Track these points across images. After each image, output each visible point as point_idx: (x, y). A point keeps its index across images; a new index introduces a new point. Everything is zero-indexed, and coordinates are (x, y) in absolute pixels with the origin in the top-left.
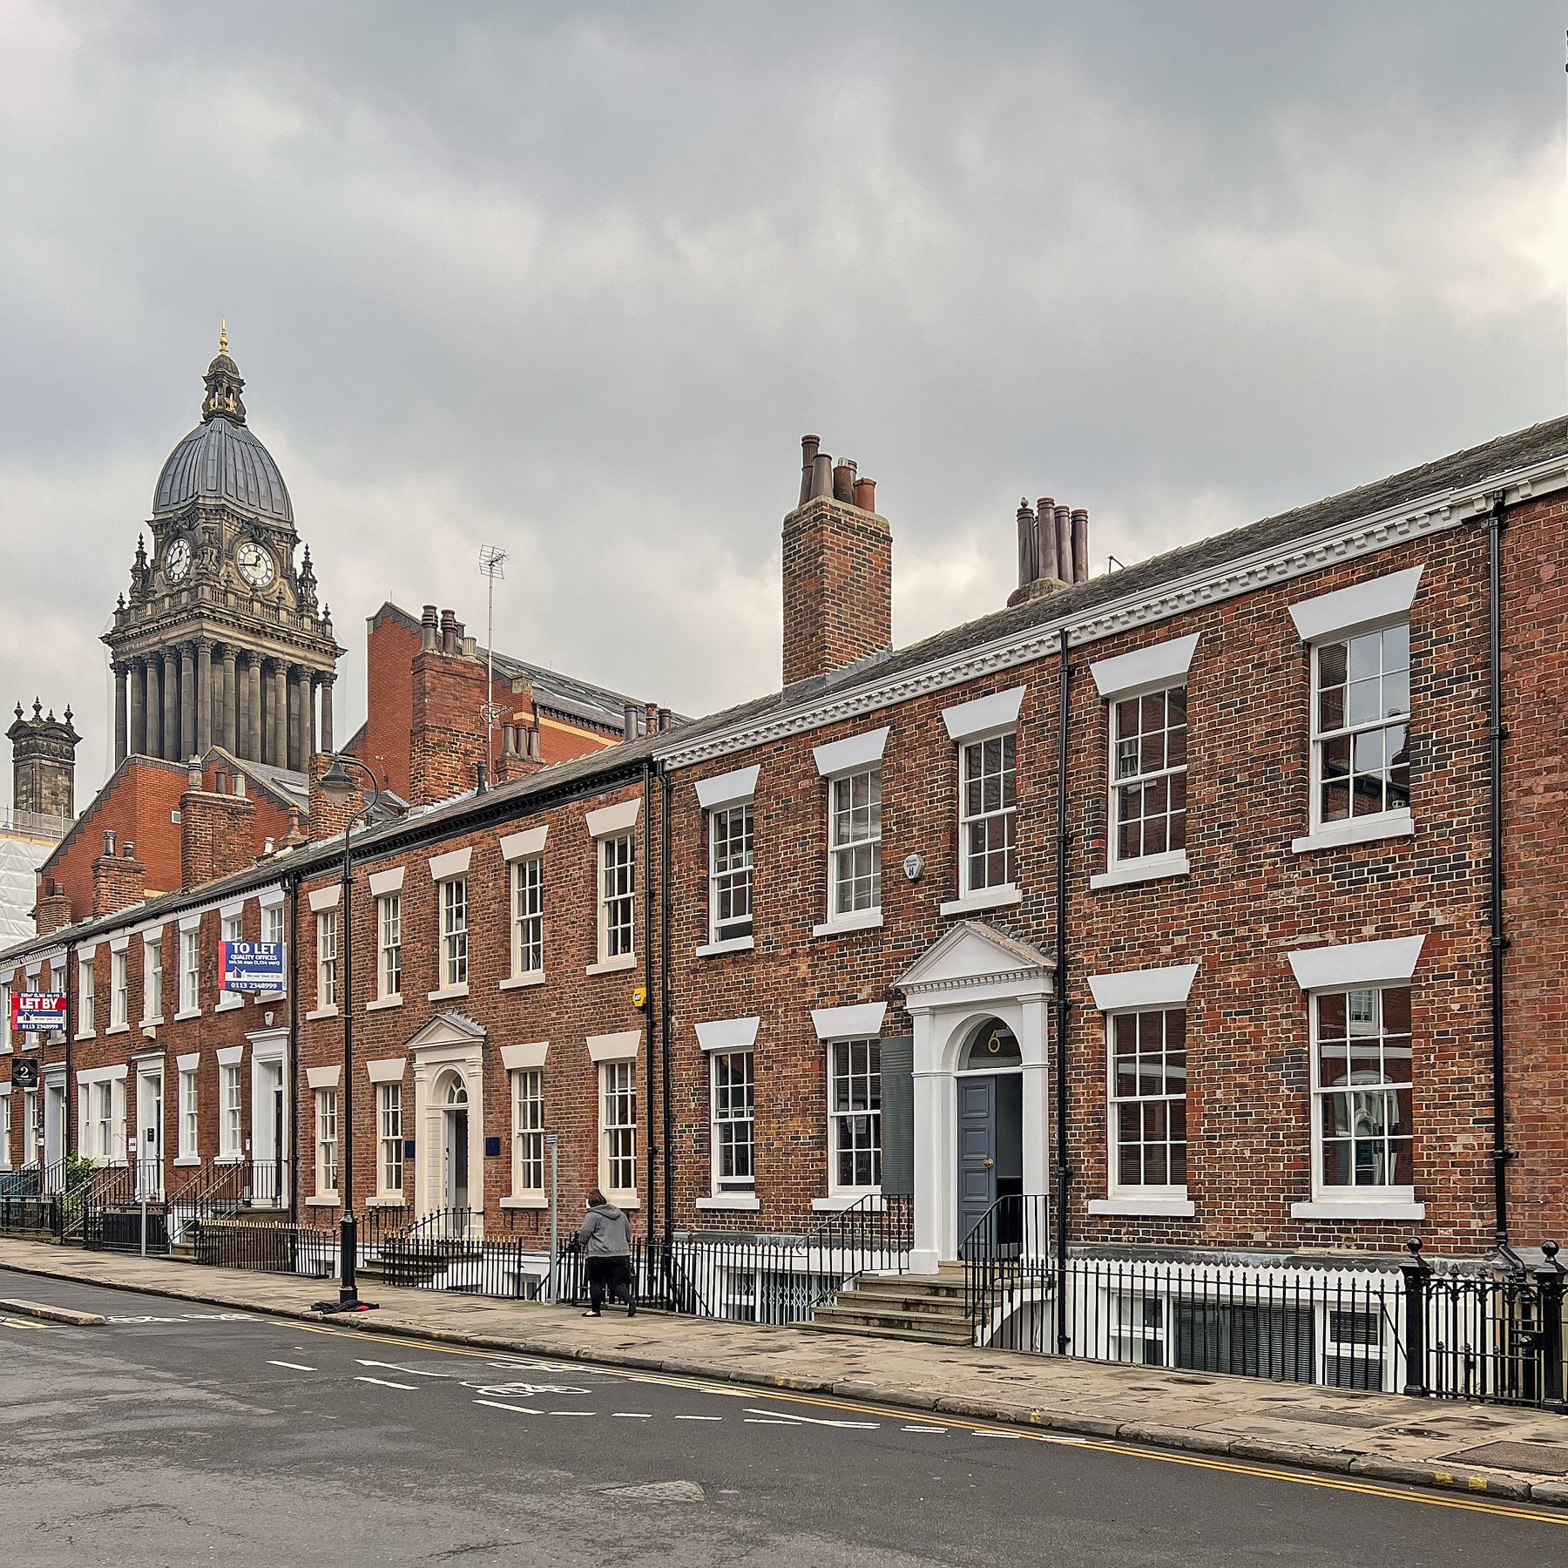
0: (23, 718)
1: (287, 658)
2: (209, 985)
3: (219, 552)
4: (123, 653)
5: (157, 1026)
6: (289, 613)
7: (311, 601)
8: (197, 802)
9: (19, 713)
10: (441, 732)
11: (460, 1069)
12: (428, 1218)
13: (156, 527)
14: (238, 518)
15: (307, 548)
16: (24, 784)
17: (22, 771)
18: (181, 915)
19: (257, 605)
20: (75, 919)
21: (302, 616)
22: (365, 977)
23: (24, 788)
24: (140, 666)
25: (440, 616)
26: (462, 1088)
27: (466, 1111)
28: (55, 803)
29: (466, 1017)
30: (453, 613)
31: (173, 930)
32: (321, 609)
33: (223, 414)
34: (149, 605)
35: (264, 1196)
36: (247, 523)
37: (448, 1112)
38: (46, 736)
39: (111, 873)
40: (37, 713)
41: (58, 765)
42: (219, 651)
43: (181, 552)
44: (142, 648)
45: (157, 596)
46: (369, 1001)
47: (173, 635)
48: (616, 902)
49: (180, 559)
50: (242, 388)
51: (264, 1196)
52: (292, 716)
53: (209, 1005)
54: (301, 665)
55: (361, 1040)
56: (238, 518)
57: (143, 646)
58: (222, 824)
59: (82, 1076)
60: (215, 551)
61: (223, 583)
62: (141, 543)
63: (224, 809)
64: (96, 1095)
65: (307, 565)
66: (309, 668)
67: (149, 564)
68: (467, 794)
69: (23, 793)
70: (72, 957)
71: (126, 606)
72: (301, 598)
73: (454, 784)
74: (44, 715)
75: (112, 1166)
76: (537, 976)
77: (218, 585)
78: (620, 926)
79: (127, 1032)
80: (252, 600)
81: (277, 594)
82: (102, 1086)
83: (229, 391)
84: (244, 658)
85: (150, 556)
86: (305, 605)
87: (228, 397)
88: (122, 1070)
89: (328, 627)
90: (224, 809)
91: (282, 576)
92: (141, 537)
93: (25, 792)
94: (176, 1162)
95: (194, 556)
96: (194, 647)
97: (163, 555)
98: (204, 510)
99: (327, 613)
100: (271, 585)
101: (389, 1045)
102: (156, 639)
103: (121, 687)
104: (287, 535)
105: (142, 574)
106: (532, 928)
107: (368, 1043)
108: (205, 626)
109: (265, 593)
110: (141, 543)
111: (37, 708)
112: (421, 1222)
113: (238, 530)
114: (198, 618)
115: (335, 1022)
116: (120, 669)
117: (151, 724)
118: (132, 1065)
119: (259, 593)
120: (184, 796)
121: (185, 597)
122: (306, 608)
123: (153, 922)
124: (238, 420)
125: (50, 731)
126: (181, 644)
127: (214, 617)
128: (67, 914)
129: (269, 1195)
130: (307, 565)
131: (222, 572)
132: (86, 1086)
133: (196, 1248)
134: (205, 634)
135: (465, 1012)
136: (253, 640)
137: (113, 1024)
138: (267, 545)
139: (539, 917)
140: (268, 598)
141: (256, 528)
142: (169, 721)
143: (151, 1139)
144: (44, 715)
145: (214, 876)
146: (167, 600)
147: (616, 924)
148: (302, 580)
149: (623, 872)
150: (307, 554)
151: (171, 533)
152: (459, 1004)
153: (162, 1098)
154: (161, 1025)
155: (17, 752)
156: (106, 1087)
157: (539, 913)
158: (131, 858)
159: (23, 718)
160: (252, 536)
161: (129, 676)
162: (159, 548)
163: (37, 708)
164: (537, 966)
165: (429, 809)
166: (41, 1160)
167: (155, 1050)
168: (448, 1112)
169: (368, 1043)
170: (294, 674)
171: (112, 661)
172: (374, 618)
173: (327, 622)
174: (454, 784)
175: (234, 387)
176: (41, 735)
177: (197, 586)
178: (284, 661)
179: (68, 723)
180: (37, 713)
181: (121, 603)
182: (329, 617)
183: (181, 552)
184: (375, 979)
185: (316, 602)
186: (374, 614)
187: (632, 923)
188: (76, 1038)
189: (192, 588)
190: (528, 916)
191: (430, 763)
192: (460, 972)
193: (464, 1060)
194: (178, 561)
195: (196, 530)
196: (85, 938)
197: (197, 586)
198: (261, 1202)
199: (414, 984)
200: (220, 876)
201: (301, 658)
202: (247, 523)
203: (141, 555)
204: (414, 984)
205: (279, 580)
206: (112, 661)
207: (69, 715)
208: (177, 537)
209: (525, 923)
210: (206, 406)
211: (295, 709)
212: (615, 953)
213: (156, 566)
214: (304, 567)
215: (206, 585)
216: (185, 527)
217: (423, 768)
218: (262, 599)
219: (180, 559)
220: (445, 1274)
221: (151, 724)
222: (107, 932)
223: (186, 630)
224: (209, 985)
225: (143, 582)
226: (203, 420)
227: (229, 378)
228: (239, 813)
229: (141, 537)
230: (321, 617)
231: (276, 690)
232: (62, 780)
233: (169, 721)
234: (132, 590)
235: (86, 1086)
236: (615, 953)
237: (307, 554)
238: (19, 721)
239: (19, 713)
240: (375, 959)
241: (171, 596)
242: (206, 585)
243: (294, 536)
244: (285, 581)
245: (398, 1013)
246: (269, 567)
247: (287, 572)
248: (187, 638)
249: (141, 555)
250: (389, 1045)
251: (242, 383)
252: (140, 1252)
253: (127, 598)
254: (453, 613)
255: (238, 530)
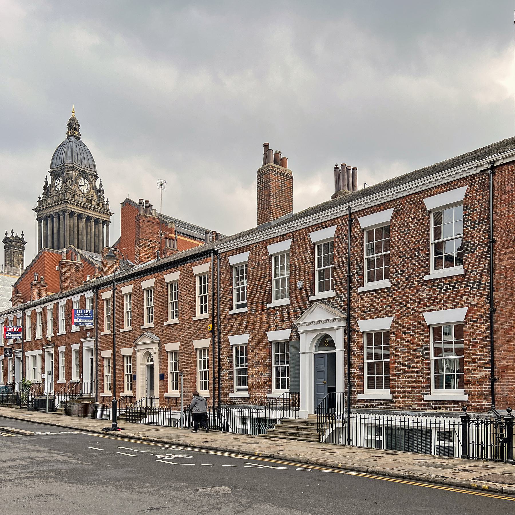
0: (7, 236)
1: (94, 216)
2: (69, 323)
3: (72, 181)
4: (40, 215)
5: (51, 337)
6: (95, 201)
7: (102, 197)
8: (65, 263)
9: (6, 234)
10: (145, 241)
11: (151, 351)
12: (141, 400)
13: (51, 173)
14: (78, 170)
15: (101, 180)
16: (8, 257)
17: (7, 253)
18: (59, 300)
19: (84, 199)
20: (25, 302)
21: (99, 202)
22: (120, 321)
23: (8, 259)
24: (46, 219)
25: (145, 202)
26: (152, 357)
27: (153, 365)
28: (18, 264)
29: (153, 334)
30: (149, 201)
31: (57, 305)
32: (105, 200)
33: (73, 136)
34: (49, 199)
35: (87, 393)
36: (81, 172)
37: (147, 365)
38: (15, 242)
39: (36, 287)
40: (12, 234)
41: (19, 251)
42: (72, 214)
43: (59, 181)
44: (47, 213)
45: (52, 196)
46: (121, 329)
47: (57, 209)
48: (202, 296)
49: (59, 184)
50: (80, 127)
51: (87, 393)
52: (96, 235)
53: (69, 330)
54: (99, 219)
55: (119, 342)
56: (78, 170)
57: (47, 212)
58: (73, 271)
59: (27, 353)
60: (71, 181)
61: (73, 191)
62: (46, 179)
63: (74, 266)
64: (32, 360)
65: (101, 186)
66: (101, 219)
67: (49, 185)
68: (154, 261)
69: (7, 260)
70: (24, 314)
71: (41, 199)
72: (99, 197)
73: (149, 258)
74: (14, 235)
75: (37, 383)
76: (176, 321)
77: (71, 192)
78: (204, 304)
79: (42, 339)
80: (83, 197)
81: (91, 195)
82: (33, 357)
83: (75, 128)
84: (80, 216)
85: (49, 183)
86: (100, 199)
87: (75, 130)
88: (40, 352)
89: (108, 206)
90: (74, 266)
91: (93, 189)
92: (46, 176)
93: (8, 260)
94: (58, 382)
95: (64, 183)
96: (64, 212)
97: (54, 182)
98: (67, 167)
99: (107, 201)
100: (89, 192)
101: (128, 343)
102: (51, 210)
103: (40, 226)
104: (94, 176)
105: (47, 189)
106: (175, 305)
107: (121, 343)
108: (67, 206)
109: (87, 195)
110: (46, 179)
111: (12, 232)
112: (138, 401)
113: (78, 174)
114: (65, 203)
115: (110, 336)
116: (39, 220)
117: (50, 238)
118: (43, 350)
119: (85, 195)
120: (60, 261)
121: (61, 196)
122: (100, 200)
123: (50, 303)
124: (78, 138)
125: (16, 240)
126: (59, 211)
127: (70, 203)
128: (22, 300)
129: (88, 393)
130: (101, 186)
131: (73, 188)
132: (28, 357)
133: (64, 410)
134: (67, 208)
135: (153, 332)
136: (83, 210)
137: (37, 336)
138: (88, 179)
139: (177, 301)
140: (88, 196)
141: (84, 173)
142: (56, 237)
143: (50, 374)
144: (14, 235)
145: (70, 288)
146: (55, 197)
147: (202, 303)
148: (99, 191)
149: (204, 286)
150: (101, 182)
151: (56, 175)
152: (151, 330)
153: (53, 361)
154: (53, 337)
155: (5, 247)
156: (35, 357)
157: (177, 300)
158: (43, 282)
159: (7, 236)
160: (83, 176)
161: (42, 222)
162: (52, 180)
163: (12, 232)
164: (176, 317)
165: (141, 266)
166: (14, 381)
167: (51, 345)
168: (147, 365)
169: (121, 343)
170: (97, 221)
171: (37, 217)
172: (123, 203)
173: (107, 204)
174: (149, 258)
175: (77, 127)
176: (13, 241)
177: (65, 193)
178: (93, 217)
179: (22, 237)
180: (12, 234)
181: (40, 198)
182: (108, 203)
183: (59, 181)
184: (123, 322)
185: (104, 198)
186: (123, 202)
187: (208, 303)
188: (25, 341)
189: (63, 193)
190: (173, 301)
191: (141, 251)
192: (151, 319)
193: (152, 348)
194: (59, 184)
195: (65, 174)
196: (28, 308)
197: (65, 193)
198: (86, 395)
199: (136, 323)
200: (72, 288)
201: (99, 216)
202: (81, 172)
203: (46, 182)
204: (136, 323)
205: (92, 190)
206: (37, 217)
207: (23, 235)
208: (58, 176)
209: (173, 303)
210: (68, 133)
211: (97, 233)
212: (202, 313)
213: (51, 186)
214: (100, 186)
215: (68, 192)
216: (61, 173)
217: (139, 252)
218: (86, 197)
219: (59, 184)
220: (146, 418)
221: (50, 238)
222: (35, 306)
223: (61, 207)
224: (69, 323)
225: (47, 191)
226: (67, 138)
227: (75, 124)
228: (79, 267)
229: (46, 176)
230: (106, 203)
231: (91, 227)
232: (20, 256)
233: (56, 237)
234: (43, 194)
235: (28, 357)
236: (202, 313)
237: (101, 182)
238: (6, 237)
239: (6, 234)
240: (123, 315)
241: (56, 196)
242: (68, 192)
243: (97, 176)
244: (94, 191)
245: (131, 333)
246: (89, 186)
247: (94, 188)
248: (61, 209)
249: (46, 182)
250: (128, 343)
251: (79, 126)
252: (46, 411)
253: (42, 196)
254: (149, 201)
255: (78, 174)
